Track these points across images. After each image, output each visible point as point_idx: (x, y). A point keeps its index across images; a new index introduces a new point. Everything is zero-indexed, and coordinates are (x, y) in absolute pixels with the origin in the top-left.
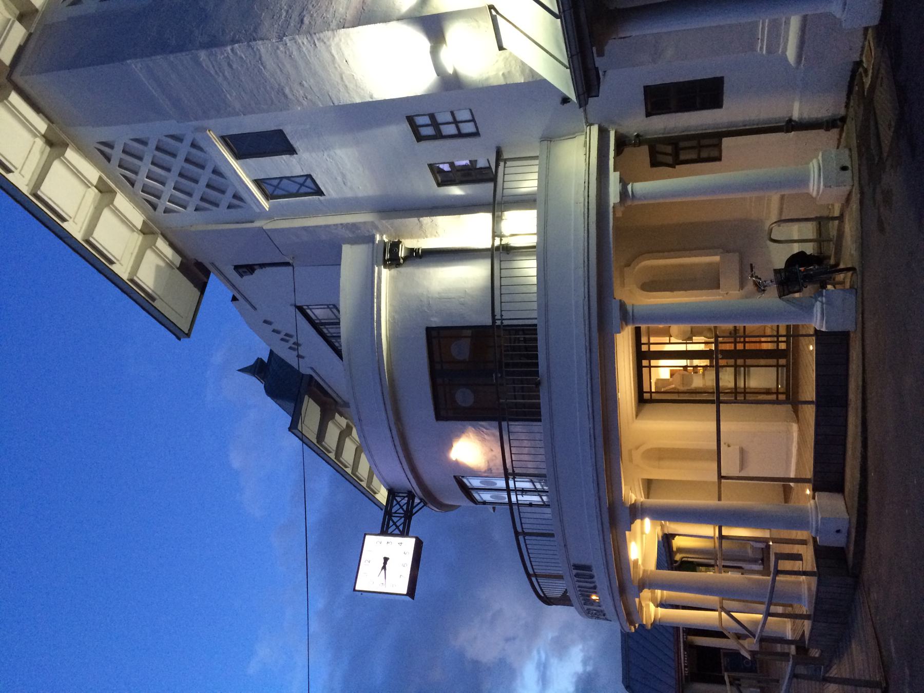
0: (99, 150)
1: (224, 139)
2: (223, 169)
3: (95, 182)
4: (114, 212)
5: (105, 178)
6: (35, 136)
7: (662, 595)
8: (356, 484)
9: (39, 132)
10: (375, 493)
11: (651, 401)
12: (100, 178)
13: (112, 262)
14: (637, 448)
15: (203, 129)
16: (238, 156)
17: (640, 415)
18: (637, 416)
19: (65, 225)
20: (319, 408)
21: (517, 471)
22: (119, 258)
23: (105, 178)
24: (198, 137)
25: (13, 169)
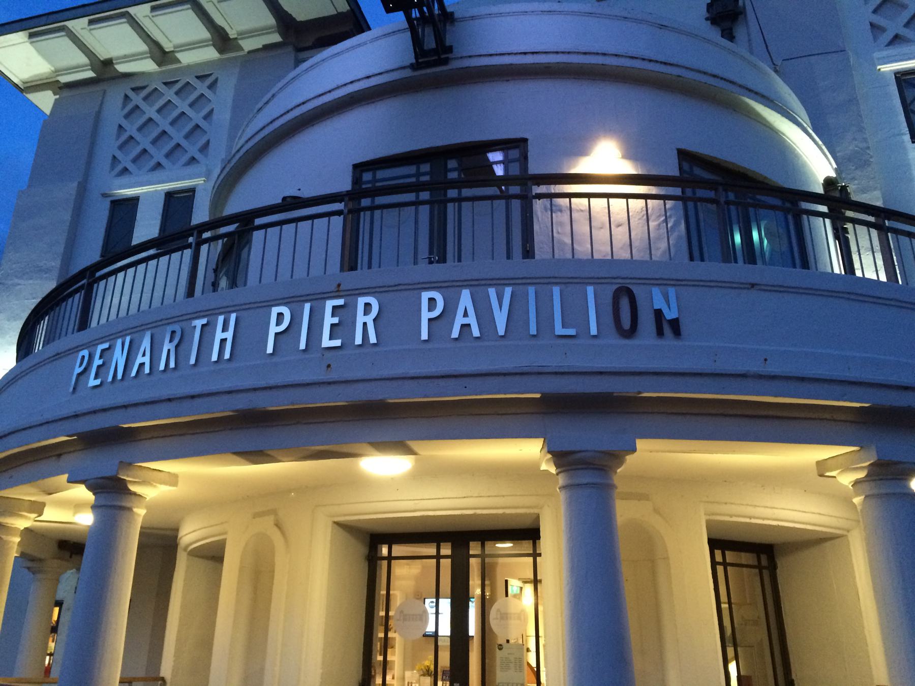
0: (211, 75)
1: (192, 190)
2: (158, 174)
3: (241, 42)
4: (142, 54)
5: (178, 65)
6: (175, 47)
7: (139, 515)
8: (31, 23)
9: (242, 39)
10: (91, 22)
11: (373, 559)
12: (178, 61)
13: (91, 22)
14: (278, 525)
15: (208, 175)
16: (169, 195)
17: (341, 533)
18: (337, 524)
19: (85, 20)
20: (298, 19)
21: (365, 217)
22: (93, 32)
23: (178, 65)
24: (200, 168)
25: (154, 14)
